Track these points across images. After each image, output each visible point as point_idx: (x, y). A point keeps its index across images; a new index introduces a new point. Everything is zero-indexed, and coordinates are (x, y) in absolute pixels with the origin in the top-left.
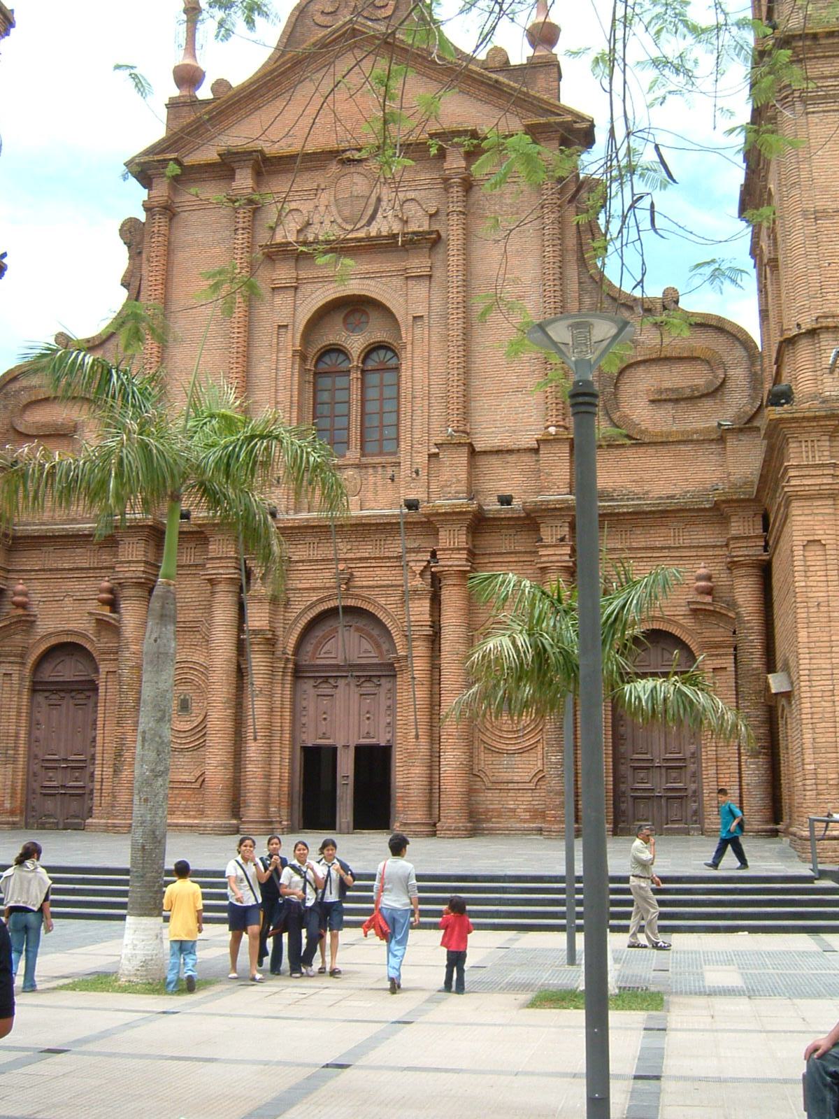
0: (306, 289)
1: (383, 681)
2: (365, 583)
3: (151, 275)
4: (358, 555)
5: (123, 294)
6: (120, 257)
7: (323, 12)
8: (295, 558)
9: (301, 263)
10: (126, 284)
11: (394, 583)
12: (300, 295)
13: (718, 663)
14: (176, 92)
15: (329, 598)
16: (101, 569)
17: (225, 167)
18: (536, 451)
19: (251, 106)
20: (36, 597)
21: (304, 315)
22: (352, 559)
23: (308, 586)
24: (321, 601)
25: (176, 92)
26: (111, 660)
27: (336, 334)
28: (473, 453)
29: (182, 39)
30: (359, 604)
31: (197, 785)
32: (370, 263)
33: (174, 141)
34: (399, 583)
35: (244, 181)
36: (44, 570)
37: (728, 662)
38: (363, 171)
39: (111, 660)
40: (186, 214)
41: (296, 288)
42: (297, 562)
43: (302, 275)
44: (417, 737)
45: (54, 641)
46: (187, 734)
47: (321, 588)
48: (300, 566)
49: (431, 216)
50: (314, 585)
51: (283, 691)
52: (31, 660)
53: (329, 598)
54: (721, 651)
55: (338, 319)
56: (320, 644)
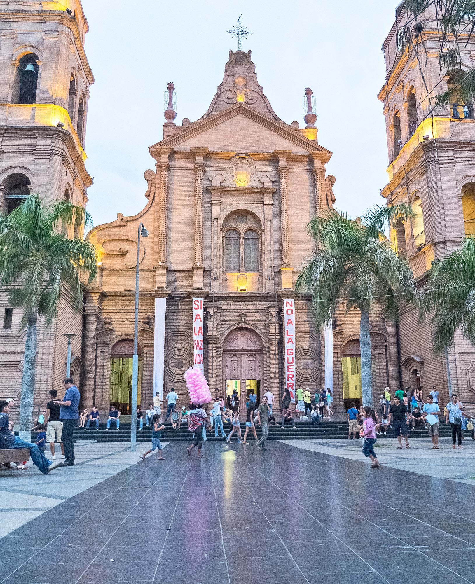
0: (224, 205)
1: (257, 356)
2: (251, 319)
3: (160, 195)
4: (248, 308)
5: (146, 201)
6: (144, 186)
7: (227, 98)
8: (223, 308)
9: (223, 195)
10: (147, 196)
11: (262, 319)
12: (222, 207)
13: (380, 351)
14: (166, 121)
15: (237, 324)
16: (142, 309)
17: (192, 154)
18: (192, 271)
19: (200, 131)
20: (113, 320)
21: (224, 215)
22: (246, 310)
23: (229, 319)
24: (234, 325)
25: (166, 121)
26: (149, 346)
27: (235, 223)
28: (168, 271)
29: (167, 100)
30: (249, 326)
31: (185, 396)
32: (249, 198)
33: (169, 140)
34: (264, 319)
35: (200, 160)
36: (117, 309)
37: (383, 351)
38: (246, 162)
39: (149, 346)
40: (173, 171)
41: (221, 204)
42: (224, 310)
43: (223, 199)
44: (275, 377)
45: (121, 338)
46: (179, 376)
47: (234, 320)
48: (225, 311)
49: (273, 182)
50: (231, 319)
51: (220, 359)
52: (111, 346)
53: (237, 324)
54: (381, 347)
55: (235, 217)
56: (233, 341)
